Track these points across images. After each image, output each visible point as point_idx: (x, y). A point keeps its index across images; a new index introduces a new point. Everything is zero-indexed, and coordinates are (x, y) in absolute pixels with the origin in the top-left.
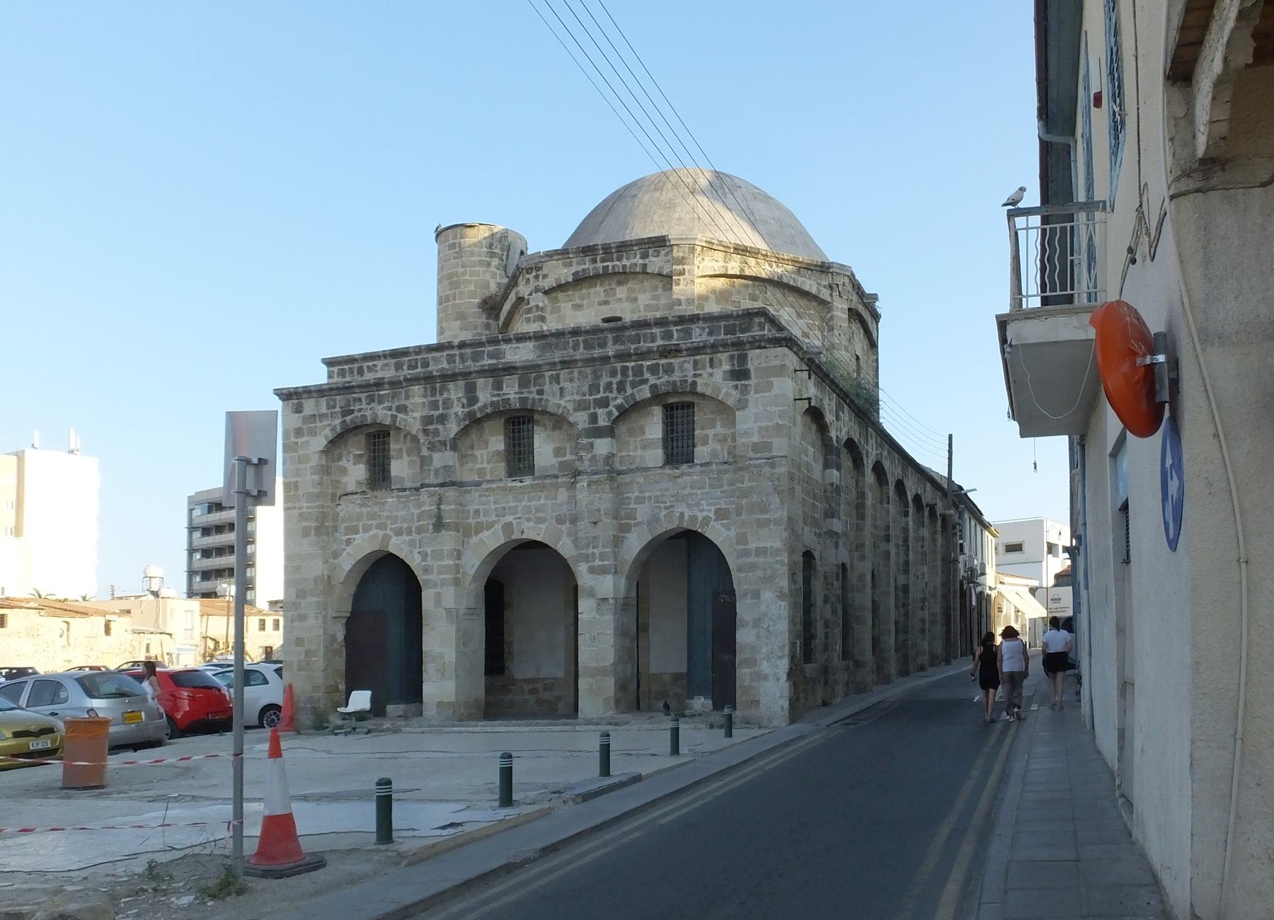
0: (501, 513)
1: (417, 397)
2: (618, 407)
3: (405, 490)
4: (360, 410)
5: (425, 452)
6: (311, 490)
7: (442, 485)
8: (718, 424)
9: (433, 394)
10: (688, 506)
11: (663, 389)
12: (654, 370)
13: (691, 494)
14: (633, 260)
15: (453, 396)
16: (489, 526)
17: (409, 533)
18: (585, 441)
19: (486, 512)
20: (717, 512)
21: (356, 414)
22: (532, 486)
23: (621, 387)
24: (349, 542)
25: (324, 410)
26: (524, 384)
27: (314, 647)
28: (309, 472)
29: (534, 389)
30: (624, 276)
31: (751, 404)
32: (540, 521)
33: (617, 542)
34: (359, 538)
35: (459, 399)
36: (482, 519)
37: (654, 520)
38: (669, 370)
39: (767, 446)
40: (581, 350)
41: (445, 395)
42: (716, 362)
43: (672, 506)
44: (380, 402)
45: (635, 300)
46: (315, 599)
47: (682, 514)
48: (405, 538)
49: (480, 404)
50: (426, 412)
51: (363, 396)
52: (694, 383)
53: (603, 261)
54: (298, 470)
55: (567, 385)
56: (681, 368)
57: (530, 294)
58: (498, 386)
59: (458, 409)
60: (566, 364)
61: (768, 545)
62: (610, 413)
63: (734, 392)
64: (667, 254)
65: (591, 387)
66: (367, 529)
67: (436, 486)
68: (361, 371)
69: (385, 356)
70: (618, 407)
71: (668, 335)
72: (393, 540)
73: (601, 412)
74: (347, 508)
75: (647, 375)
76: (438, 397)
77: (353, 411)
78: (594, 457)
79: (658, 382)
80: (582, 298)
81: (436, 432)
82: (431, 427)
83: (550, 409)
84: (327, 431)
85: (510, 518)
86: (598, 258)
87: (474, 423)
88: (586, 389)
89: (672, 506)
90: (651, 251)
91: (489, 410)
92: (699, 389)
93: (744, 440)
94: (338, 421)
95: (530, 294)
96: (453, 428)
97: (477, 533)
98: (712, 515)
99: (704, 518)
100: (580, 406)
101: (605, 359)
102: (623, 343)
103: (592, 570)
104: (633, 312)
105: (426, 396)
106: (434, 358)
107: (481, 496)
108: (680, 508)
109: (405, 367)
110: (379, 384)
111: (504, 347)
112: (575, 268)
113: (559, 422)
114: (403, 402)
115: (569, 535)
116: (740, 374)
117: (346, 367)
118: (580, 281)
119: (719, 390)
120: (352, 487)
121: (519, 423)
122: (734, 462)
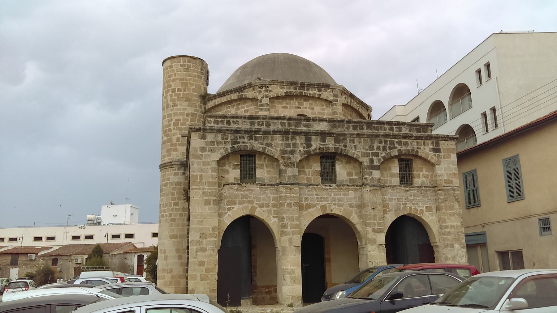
0: (320, 200)
1: (278, 140)
3: (265, 185)
4: (243, 142)
5: (282, 167)
6: (211, 180)
7: (292, 184)
8: (424, 170)
10: (413, 204)
11: (404, 152)
12: (399, 143)
13: (413, 199)
14: (314, 92)
15: (298, 142)
16: (314, 206)
17: (268, 206)
18: (368, 171)
19: (311, 199)
20: (427, 207)
21: (241, 144)
22: (336, 189)
23: (384, 149)
24: (229, 209)
25: (220, 139)
26: (337, 141)
27: (211, 266)
28: (210, 171)
29: (342, 144)
30: (307, 98)
31: (442, 163)
32: (340, 205)
33: (383, 218)
34: (236, 207)
35: (302, 144)
37: (398, 209)
38: (406, 144)
39: (451, 182)
40: (351, 130)
41: (294, 141)
42: (426, 144)
43: (406, 204)
45: (313, 109)
46: (212, 239)
47: (411, 208)
48: (265, 209)
50: (284, 148)
51: (245, 136)
52: (417, 151)
55: (358, 144)
56: (411, 144)
57: (262, 98)
58: (323, 140)
61: (455, 224)
62: (379, 160)
63: (434, 157)
64: (330, 92)
65: (370, 147)
66: (240, 203)
68: (228, 123)
69: (245, 118)
70: (383, 157)
71: (391, 129)
72: (258, 209)
73: (375, 158)
74: (226, 191)
75: (396, 145)
76: (290, 142)
77: (239, 143)
78: (372, 178)
79: (402, 149)
80: (287, 104)
81: (289, 158)
82: (286, 156)
83: (349, 154)
85: (325, 203)
86: (298, 88)
87: (388, 159)
88: (367, 147)
89: (406, 204)
90: (322, 89)
91: (318, 151)
92: (419, 154)
93: (441, 178)
94: (229, 147)
95: (262, 98)
96: (298, 157)
97: (307, 209)
98: (424, 209)
99: (421, 210)
100: (365, 155)
101: (378, 136)
102: (371, 129)
103: (374, 231)
104: (312, 113)
105: (283, 140)
106: (273, 122)
107: (308, 191)
108: (409, 205)
109: (256, 125)
111: (312, 123)
112: (285, 90)
113: (351, 160)
114: (269, 141)
115: (356, 213)
116: (437, 150)
117: (220, 120)
120: (231, 180)
121: (328, 159)
122: (435, 187)
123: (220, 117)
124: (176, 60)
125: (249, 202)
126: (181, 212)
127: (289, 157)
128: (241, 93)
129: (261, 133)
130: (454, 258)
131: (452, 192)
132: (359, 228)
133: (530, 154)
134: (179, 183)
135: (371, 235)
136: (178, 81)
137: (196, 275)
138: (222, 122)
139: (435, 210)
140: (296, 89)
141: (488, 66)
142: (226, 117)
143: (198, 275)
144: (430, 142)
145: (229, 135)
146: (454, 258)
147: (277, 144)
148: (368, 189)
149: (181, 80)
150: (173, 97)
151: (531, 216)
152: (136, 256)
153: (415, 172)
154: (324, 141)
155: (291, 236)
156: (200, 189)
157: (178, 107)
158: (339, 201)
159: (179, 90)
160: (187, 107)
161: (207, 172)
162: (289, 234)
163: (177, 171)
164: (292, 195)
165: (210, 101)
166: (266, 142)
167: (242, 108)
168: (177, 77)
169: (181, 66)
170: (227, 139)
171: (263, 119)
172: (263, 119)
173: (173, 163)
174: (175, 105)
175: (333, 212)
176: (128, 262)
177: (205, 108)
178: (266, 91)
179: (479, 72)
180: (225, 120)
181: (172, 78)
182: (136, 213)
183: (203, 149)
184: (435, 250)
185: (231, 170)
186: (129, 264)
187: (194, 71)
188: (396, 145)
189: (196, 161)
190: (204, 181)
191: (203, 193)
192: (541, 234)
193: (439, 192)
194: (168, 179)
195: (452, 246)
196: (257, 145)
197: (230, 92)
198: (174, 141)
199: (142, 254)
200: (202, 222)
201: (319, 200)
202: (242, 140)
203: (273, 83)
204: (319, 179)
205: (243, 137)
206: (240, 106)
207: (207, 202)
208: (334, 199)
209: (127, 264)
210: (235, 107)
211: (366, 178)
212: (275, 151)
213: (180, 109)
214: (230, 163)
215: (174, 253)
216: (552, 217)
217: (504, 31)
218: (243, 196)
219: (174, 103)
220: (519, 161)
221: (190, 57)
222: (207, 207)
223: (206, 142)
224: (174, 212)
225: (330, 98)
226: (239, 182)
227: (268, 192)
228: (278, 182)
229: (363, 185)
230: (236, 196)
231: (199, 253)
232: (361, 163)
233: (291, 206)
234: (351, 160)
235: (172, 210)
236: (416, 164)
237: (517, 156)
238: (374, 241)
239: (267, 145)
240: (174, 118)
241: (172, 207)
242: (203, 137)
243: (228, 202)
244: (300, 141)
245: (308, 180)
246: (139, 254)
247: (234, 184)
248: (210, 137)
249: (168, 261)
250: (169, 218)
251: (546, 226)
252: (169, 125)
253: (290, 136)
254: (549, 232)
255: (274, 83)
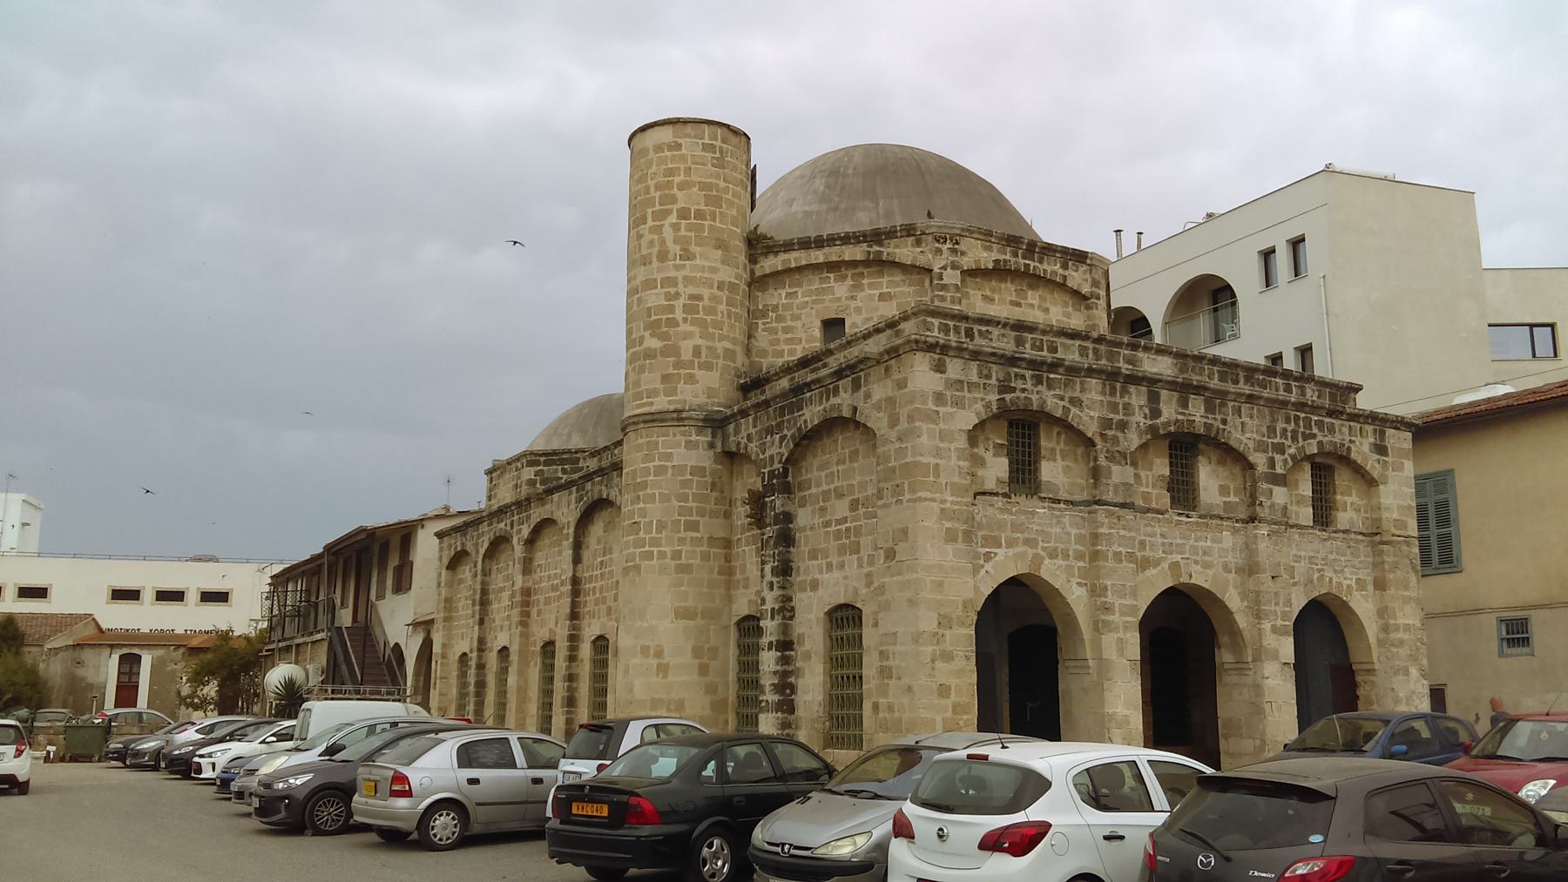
1: (1094, 391)
2: (1293, 457)
3: (1059, 501)
4: (1024, 390)
6: (957, 479)
7: (1123, 506)
9: (1113, 394)
11: (1328, 448)
12: (1320, 424)
13: (1335, 560)
14: (1051, 267)
16: (1157, 563)
18: (1265, 486)
21: (1018, 394)
23: (1295, 439)
24: (988, 557)
26: (1210, 408)
27: (964, 700)
29: (1219, 417)
30: (1037, 280)
32: (1207, 566)
35: (1141, 407)
36: (1148, 553)
37: (1309, 582)
44: (1050, 387)
45: (1046, 310)
49: (1162, 419)
51: (1028, 374)
53: (1024, 257)
54: (938, 449)
57: (944, 268)
58: (1184, 403)
59: (1139, 419)
60: (1251, 398)
66: (1010, 545)
67: (1115, 505)
69: (1005, 325)
70: (1293, 457)
72: (1047, 561)
73: (1278, 457)
75: (1315, 431)
77: (1013, 390)
78: (1273, 505)
81: (1115, 440)
82: (1110, 433)
83: (1232, 443)
84: (979, 406)
85: (1178, 558)
88: (1264, 429)
91: (1172, 429)
94: (993, 397)
100: (1261, 447)
103: (1275, 630)
105: (1104, 393)
110: (1054, 366)
111: (1140, 354)
112: (995, 255)
113: (1232, 456)
114: (1077, 394)
115: (1235, 587)
117: (951, 323)
118: (999, 272)
119: (1366, 459)
120: (990, 485)
121: (1183, 448)
123: (953, 317)
124: (689, 129)
125: (1027, 542)
126: (705, 548)
127: (1115, 437)
128: (876, 248)
129: (1061, 370)
130: (1409, 699)
131: (1404, 548)
132: (1242, 621)
133: (1484, 475)
134: (698, 471)
135: (1270, 640)
136: (695, 189)
137: (933, 720)
138: (956, 329)
139: (1371, 588)
140: (1016, 255)
141: (1296, 243)
142: (966, 318)
143: (939, 719)
144: (1369, 428)
145: (995, 368)
146: (1409, 699)
147: (1093, 402)
148: (1263, 530)
149: (704, 187)
150: (683, 232)
151: (1477, 611)
152: (115, 658)
153: (1339, 497)
154: (1186, 406)
155: (1120, 635)
156: (933, 500)
157: (698, 262)
158: (1204, 557)
159: (699, 215)
160: (719, 265)
161: (950, 458)
162: (1116, 630)
163: (694, 438)
164: (1122, 532)
165: (771, 257)
166: (1069, 394)
167: (871, 286)
168: (694, 178)
169: (706, 148)
170: (988, 377)
171: (1044, 332)
172: (1044, 332)
173: (684, 415)
174: (687, 255)
175: (1193, 581)
176: (87, 674)
177: (752, 272)
178: (953, 251)
179: (1268, 255)
180: (963, 325)
181: (677, 180)
182: (36, 519)
183: (939, 398)
184: (1359, 679)
185: (989, 456)
186: (90, 680)
187: (735, 169)
188: (1315, 431)
189: (925, 427)
190: (943, 480)
191: (943, 510)
192: (1501, 654)
193: (1385, 547)
194: (669, 457)
195: (1407, 673)
196: (1052, 401)
197: (840, 238)
198: (686, 355)
199: (136, 651)
200: (941, 584)
201: (1167, 548)
202: (1019, 384)
203: (969, 232)
204: (1166, 499)
205: (1023, 377)
206: (865, 281)
207: (951, 537)
208: (1194, 550)
209: (83, 679)
210: (849, 282)
211: (1261, 504)
212: (1088, 419)
213: (702, 269)
214: (988, 439)
215: (687, 658)
216: (1536, 618)
217: (1338, 166)
218: (1016, 527)
219: (685, 250)
220: (1453, 485)
221: (728, 126)
222: (950, 548)
223: (947, 380)
224: (686, 548)
225: (1086, 289)
226: (1007, 490)
227: (1066, 520)
228: (1085, 496)
229: (1252, 519)
230: (1001, 526)
231: (939, 664)
232: (1251, 466)
233: (1121, 561)
234: (1232, 456)
235: (681, 541)
236: (1342, 478)
237: (1452, 471)
238: (1275, 655)
239: (1073, 401)
240: (686, 291)
241: (682, 535)
242: (940, 368)
243: (985, 538)
244: (1137, 398)
245: (1146, 497)
246: (125, 651)
247: (996, 494)
248: (954, 368)
249: (670, 678)
250: (673, 563)
251: (1516, 633)
252: (671, 309)
253: (1118, 385)
254: (1525, 650)
255: (972, 232)
